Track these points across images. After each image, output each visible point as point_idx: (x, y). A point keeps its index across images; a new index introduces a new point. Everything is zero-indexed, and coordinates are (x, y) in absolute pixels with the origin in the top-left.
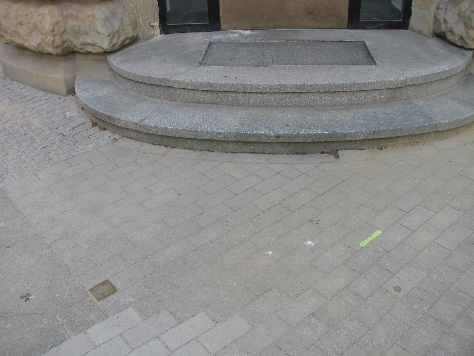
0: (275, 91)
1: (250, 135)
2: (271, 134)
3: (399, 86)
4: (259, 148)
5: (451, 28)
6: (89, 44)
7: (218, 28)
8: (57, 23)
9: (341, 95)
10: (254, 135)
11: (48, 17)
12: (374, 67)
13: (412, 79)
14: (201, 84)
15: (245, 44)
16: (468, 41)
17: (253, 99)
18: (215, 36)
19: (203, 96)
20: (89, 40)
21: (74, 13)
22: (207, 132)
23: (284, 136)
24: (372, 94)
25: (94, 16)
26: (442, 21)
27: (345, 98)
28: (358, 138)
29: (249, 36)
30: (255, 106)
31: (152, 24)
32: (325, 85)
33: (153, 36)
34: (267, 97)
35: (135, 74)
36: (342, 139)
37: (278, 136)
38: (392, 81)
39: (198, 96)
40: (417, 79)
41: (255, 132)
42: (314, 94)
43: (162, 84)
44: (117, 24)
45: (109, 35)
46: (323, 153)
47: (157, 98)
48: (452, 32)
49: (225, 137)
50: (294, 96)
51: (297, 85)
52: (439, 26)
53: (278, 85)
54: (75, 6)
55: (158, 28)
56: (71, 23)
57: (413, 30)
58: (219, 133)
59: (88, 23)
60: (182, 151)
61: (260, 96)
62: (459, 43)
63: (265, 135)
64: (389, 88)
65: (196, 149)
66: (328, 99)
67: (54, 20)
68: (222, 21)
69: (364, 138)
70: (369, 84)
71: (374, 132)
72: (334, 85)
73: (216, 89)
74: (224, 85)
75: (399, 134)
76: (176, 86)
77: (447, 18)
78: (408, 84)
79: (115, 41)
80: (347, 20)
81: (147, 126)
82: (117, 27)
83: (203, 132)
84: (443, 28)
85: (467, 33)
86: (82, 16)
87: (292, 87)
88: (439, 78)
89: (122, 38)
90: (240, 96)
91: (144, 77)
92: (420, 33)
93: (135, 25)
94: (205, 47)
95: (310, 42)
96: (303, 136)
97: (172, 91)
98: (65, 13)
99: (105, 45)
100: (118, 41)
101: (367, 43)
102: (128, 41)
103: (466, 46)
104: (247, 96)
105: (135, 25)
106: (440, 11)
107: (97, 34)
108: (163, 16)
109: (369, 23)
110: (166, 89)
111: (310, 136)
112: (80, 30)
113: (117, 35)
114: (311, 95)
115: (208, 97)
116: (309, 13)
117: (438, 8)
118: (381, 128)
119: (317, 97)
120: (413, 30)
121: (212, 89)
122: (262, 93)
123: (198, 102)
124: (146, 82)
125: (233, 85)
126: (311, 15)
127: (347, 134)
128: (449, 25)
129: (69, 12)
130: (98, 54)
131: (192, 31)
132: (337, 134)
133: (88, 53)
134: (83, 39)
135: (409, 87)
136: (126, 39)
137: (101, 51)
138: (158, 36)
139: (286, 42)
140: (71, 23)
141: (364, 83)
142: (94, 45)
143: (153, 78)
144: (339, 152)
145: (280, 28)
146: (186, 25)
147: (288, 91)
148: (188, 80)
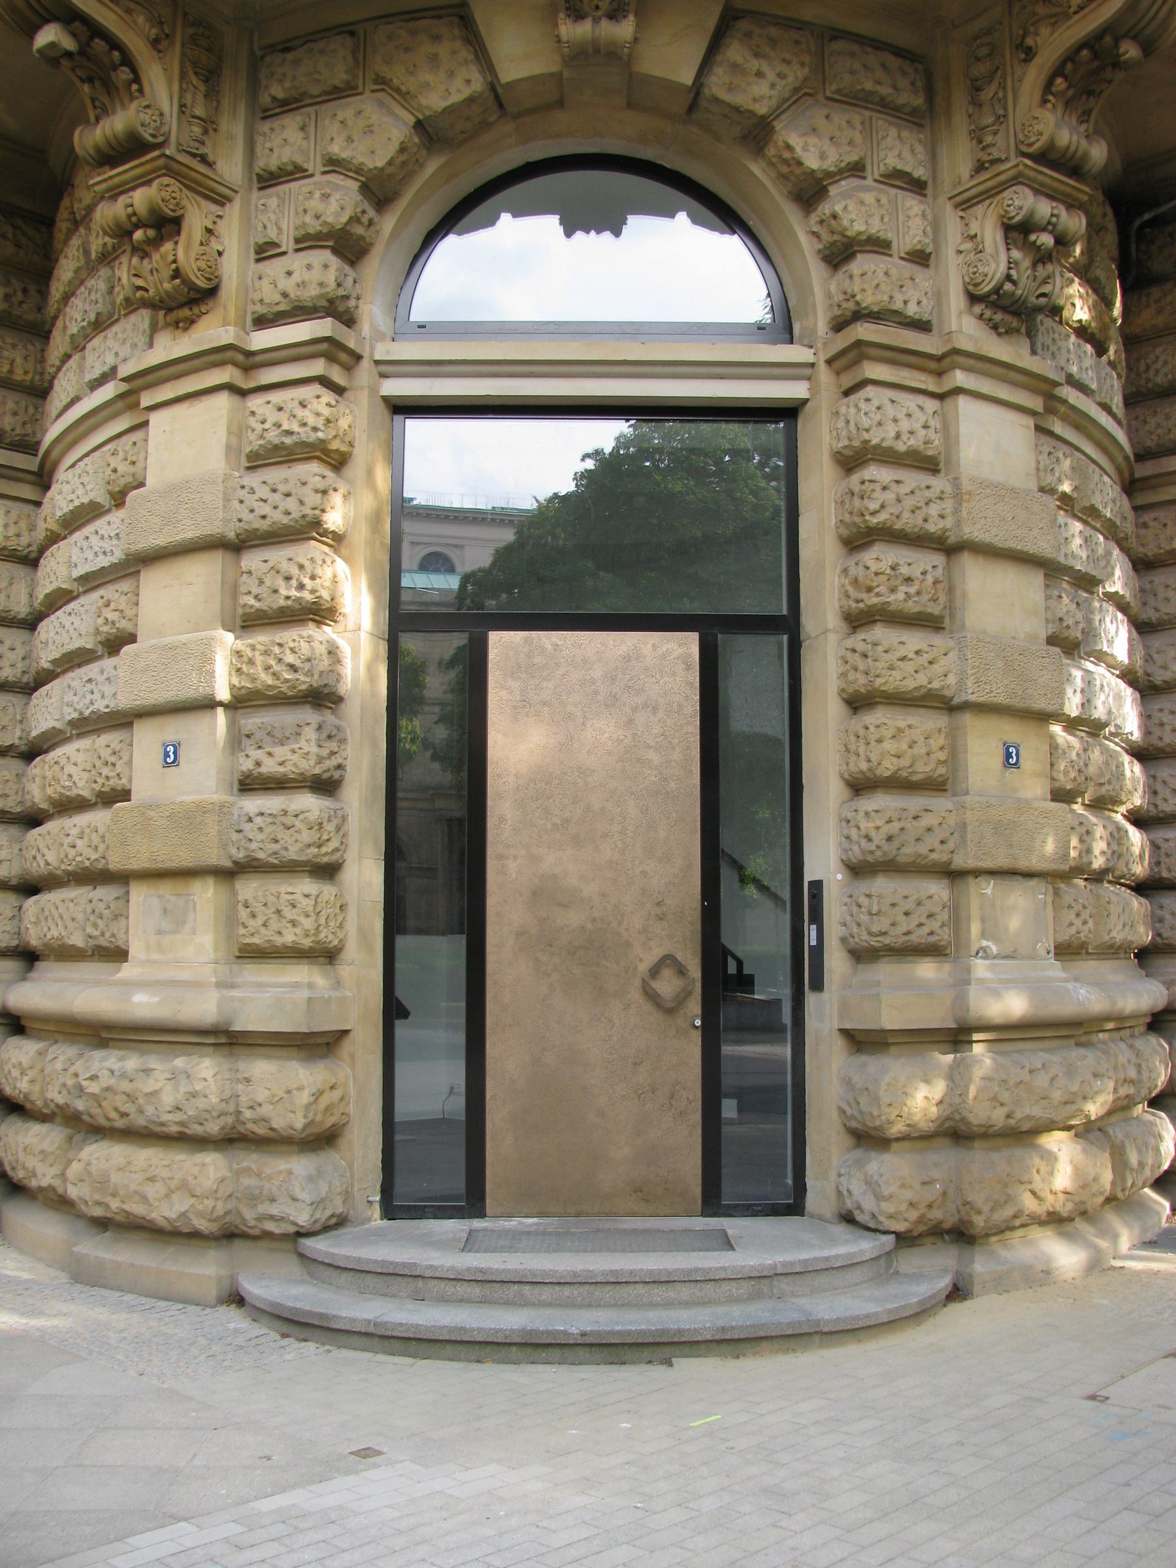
0: (579, 1280)
1: (542, 1333)
2: (574, 1330)
3: (764, 1274)
4: (556, 1353)
5: (858, 1202)
6: (272, 1218)
7: (482, 1215)
8: (223, 1180)
9: (678, 1286)
10: (549, 1333)
11: (211, 1170)
12: (730, 1252)
13: (784, 1264)
14: (468, 1269)
15: (529, 1233)
16: (882, 1218)
17: (546, 1293)
18: (477, 1224)
19: (469, 1290)
20: (274, 1210)
21: (253, 1166)
22: (480, 1330)
23: (592, 1333)
24: (726, 1287)
25: (290, 1172)
26: (845, 1193)
27: (685, 1292)
28: (699, 1338)
29: (534, 1224)
30: (549, 1305)
31: (370, 1199)
32: (652, 1271)
33: (369, 1220)
34: (567, 1291)
35: (359, 1259)
36: (676, 1339)
37: (583, 1334)
38: (752, 1266)
39: (461, 1289)
40: (792, 1264)
41: (550, 1328)
42: (637, 1286)
43: (406, 1272)
44: (324, 1189)
45: (312, 1204)
46: (650, 1362)
47: (394, 1296)
48: (859, 1208)
49: (506, 1337)
50: (608, 1288)
51: (611, 1271)
52: (844, 1204)
53: (583, 1271)
54: (254, 1156)
55: (377, 1207)
56: (246, 1181)
57: (812, 1216)
58: (497, 1331)
59: (277, 1183)
60: (438, 1362)
61: (557, 1288)
62: (872, 1225)
63: (565, 1333)
64: (750, 1278)
65: (460, 1360)
66: (658, 1293)
67: (219, 1175)
68: (488, 1201)
69: (709, 1337)
70: (717, 1269)
71: (723, 1329)
72: (667, 1271)
73: (490, 1278)
74: (504, 1270)
75: (762, 1334)
76: (428, 1273)
77: (851, 1187)
78: (778, 1272)
79: (317, 1216)
80: (700, 1202)
81: (386, 1323)
82: (323, 1194)
83: (473, 1329)
84: (849, 1204)
85: (879, 1206)
86: (269, 1172)
87: (604, 1273)
88: (828, 1265)
89: (328, 1213)
90: (526, 1289)
91: (376, 1261)
92: (820, 1218)
93: (347, 1195)
94: (466, 1235)
95: (635, 1231)
96: (620, 1333)
97: (420, 1283)
98: (235, 1166)
99: (303, 1218)
100: (323, 1215)
101: (730, 1232)
102: (333, 1221)
103: (881, 1228)
104: (537, 1289)
105: (347, 1195)
106: (842, 1179)
107: (290, 1201)
108: (387, 1190)
109: (737, 1205)
110: (410, 1279)
111: (629, 1333)
112: (261, 1193)
113: (321, 1206)
114: (632, 1286)
115: (476, 1291)
116: (637, 1190)
117: (840, 1175)
118: (734, 1324)
119: (641, 1289)
120: (812, 1216)
121: (485, 1278)
122: (559, 1283)
123: (461, 1301)
124: (379, 1270)
125: (516, 1271)
126: (640, 1194)
127: (684, 1330)
128: (855, 1198)
129: (244, 1164)
130: (285, 1237)
131: (435, 1217)
132: (668, 1331)
133: (267, 1235)
134: (264, 1208)
135: (782, 1278)
136: (332, 1216)
137: (292, 1229)
138: (376, 1220)
139: (598, 1231)
140: (246, 1181)
141: (710, 1269)
142: (282, 1219)
143: (391, 1263)
144: (674, 1360)
145: (588, 1215)
146: (425, 1206)
147: (599, 1279)
148: (448, 1265)
